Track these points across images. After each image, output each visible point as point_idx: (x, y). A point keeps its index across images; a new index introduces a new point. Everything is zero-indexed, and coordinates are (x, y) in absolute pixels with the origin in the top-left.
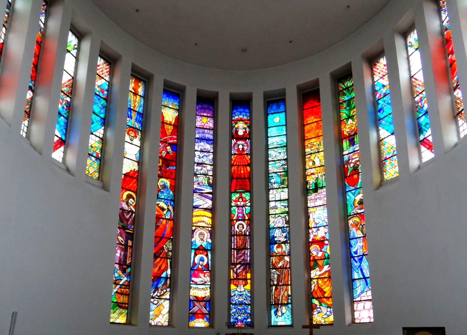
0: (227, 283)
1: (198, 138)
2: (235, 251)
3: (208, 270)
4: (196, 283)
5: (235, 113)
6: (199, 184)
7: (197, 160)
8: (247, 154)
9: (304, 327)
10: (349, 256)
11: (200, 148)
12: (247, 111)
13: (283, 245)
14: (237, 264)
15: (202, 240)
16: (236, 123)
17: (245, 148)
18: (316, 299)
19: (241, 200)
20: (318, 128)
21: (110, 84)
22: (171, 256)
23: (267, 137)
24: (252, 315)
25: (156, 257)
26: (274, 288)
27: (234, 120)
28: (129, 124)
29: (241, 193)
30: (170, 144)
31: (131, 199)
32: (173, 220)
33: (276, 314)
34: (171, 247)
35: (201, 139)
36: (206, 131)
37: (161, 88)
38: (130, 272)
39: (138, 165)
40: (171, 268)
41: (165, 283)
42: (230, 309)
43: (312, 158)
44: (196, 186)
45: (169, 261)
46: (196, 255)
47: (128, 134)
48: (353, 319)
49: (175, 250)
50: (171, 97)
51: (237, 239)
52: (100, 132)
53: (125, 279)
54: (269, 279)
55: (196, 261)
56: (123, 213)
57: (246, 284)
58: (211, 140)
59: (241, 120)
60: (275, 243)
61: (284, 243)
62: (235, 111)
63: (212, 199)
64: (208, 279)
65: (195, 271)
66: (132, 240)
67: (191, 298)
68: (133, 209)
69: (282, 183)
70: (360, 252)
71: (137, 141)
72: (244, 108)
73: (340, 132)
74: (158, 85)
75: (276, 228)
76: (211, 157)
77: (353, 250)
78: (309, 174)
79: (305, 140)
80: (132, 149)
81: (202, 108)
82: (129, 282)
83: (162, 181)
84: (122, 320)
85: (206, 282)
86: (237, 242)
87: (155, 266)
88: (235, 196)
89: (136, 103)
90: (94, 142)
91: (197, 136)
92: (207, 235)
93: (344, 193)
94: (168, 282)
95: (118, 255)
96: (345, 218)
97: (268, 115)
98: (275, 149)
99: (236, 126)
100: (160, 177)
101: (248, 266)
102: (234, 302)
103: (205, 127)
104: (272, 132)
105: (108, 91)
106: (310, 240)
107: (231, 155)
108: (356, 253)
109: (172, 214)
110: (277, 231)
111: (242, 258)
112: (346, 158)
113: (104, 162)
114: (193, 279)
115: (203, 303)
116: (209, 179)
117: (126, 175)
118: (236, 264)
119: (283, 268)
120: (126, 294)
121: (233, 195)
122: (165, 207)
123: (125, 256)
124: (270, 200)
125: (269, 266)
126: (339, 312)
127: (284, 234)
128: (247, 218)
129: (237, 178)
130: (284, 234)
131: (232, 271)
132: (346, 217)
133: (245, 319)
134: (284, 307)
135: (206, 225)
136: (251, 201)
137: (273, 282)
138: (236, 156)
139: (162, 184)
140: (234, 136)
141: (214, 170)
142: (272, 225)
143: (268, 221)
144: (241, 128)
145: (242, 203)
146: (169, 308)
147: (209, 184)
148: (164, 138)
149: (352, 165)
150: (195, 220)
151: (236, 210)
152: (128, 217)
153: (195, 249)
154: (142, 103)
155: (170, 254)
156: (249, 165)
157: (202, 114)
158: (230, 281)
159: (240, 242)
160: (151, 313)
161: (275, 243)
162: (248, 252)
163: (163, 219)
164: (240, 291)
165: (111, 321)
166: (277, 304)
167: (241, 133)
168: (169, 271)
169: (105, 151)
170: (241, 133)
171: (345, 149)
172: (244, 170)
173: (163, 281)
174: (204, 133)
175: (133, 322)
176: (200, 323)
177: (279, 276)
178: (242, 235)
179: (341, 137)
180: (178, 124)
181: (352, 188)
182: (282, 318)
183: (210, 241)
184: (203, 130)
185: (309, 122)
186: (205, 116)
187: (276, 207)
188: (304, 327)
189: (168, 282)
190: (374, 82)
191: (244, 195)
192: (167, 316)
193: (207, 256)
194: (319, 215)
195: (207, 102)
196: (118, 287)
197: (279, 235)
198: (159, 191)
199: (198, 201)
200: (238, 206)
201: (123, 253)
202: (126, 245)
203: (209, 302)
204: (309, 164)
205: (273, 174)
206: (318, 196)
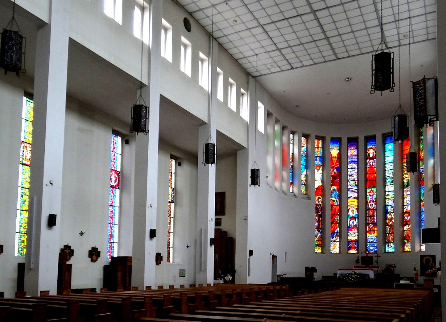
1: (349, 162)
2: (369, 218)
3: (356, 227)
4: (351, 234)
5: (368, 145)
6: (350, 186)
7: (349, 173)
8: (375, 167)
9: (380, 256)
11: (351, 166)
12: (374, 143)
13: (392, 214)
15: (353, 213)
16: (369, 150)
17: (374, 164)
19: (371, 192)
21: (307, 147)
22: (339, 222)
25: (332, 223)
26: (387, 234)
27: (368, 149)
28: (316, 164)
29: (371, 188)
30: (336, 168)
31: (320, 199)
32: (339, 205)
33: (388, 247)
34: (339, 218)
35: (351, 162)
36: (353, 157)
37: (330, 139)
38: (321, 231)
39: (322, 182)
40: (339, 228)
41: (337, 235)
44: (349, 187)
45: (338, 225)
46: (350, 220)
47: (316, 169)
49: (340, 220)
50: (335, 143)
51: (370, 212)
52: (304, 173)
53: (319, 234)
55: (351, 224)
56: (317, 206)
57: (374, 233)
58: (356, 161)
59: (371, 148)
60: (388, 213)
61: (393, 213)
64: (356, 231)
65: (349, 228)
67: (349, 240)
68: (321, 204)
71: (320, 171)
72: (373, 142)
74: (328, 140)
75: (389, 205)
76: (356, 170)
78: (405, 177)
80: (318, 175)
82: (321, 235)
83: (333, 188)
84: (320, 251)
85: (355, 233)
86: (370, 213)
87: (332, 227)
90: (303, 178)
91: (349, 161)
92: (355, 211)
94: (338, 234)
95: (316, 225)
96: (419, 201)
97: (385, 144)
98: (388, 164)
99: (369, 152)
100: (332, 185)
102: (369, 242)
103: (353, 155)
104: (387, 154)
105: (306, 151)
106: (405, 211)
108: (423, 219)
109: (338, 202)
110: (389, 207)
111: (372, 221)
113: (307, 186)
116: (356, 183)
118: (369, 224)
119: (392, 225)
120: (321, 241)
121: (368, 189)
122: (335, 200)
123: (319, 225)
124: (386, 191)
127: (393, 209)
128: (374, 201)
129: (370, 181)
130: (393, 209)
131: (368, 227)
133: (374, 249)
134: (392, 244)
135: (355, 206)
137: (387, 232)
138: (369, 168)
139: (333, 189)
141: (358, 178)
142: (387, 204)
145: (372, 193)
146: (339, 245)
147: (356, 185)
148: (333, 166)
150: (349, 204)
151: (369, 197)
152: (319, 207)
153: (350, 218)
154: (321, 151)
155: (338, 221)
157: (351, 148)
160: (331, 248)
161: (388, 213)
163: (334, 205)
164: (372, 237)
165: (315, 252)
166: (389, 242)
167: (371, 156)
168: (338, 229)
169: (307, 181)
170: (371, 156)
171: (421, 166)
172: (373, 176)
174: (352, 158)
175: (324, 252)
176: (353, 251)
177: (390, 229)
178: (372, 210)
183: (357, 213)
184: (352, 157)
185: (406, 149)
186: (353, 149)
187: (388, 195)
188: (380, 256)
189: (338, 234)
191: (373, 189)
192: (338, 249)
193: (356, 220)
195: (353, 142)
196: (317, 238)
197: (390, 209)
198: (332, 192)
199: (350, 194)
201: (318, 224)
203: (357, 242)
205: (388, 178)
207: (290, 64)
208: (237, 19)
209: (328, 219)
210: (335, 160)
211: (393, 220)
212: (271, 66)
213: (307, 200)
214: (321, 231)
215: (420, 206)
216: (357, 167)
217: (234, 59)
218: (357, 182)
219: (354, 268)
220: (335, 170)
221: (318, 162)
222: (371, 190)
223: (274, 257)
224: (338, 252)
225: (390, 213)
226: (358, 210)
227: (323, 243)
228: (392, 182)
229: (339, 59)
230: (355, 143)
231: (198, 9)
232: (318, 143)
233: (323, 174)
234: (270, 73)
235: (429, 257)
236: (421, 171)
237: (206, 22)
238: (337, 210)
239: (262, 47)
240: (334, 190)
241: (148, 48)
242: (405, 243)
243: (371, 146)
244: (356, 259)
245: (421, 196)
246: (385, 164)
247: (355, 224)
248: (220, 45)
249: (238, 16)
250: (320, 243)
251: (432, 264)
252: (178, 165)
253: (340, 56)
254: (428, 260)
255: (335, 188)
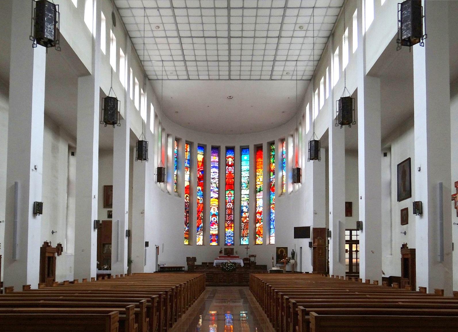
0: (224, 228)
4: (212, 229)
9: (249, 248)
10: (270, 220)
12: (233, 153)
13: (246, 213)
14: (228, 221)
16: (228, 159)
17: (232, 170)
18: (258, 235)
20: (262, 164)
23: (241, 166)
24: (233, 240)
30: (201, 171)
35: (214, 167)
36: (215, 163)
37: (197, 145)
42: (225, 238)
43: (259, 177)
44: (212, 188)
45: (202, 220)
46: (212, 217)
48: (270, 242)
53: (187, 228)
54: (241, 227)
55: (212, 220)
57: (232, 228)
59: (230, 157)
61: (247, 212)
62: (227, 153)
63: (218, 194)
64: (217, 227)
66: (188, 214)
68: (188, 201)
69: (247, 187)
70: (274, 218)
71: (188, 173)
72: (232, 151)
73: (270, 168)
74: (196, 146)
77: (271, 217)
79: (256, 169)
81: (213, 152)
88: (227, 192)
89: (187, 155)
91: (212, 166)
92: (216, 209)
93: (270, 194)
94: (202, 228)
97: (242, 155)
99: (228, 160)
101: (232, 221)
106: (257, 212)
107: (226, 174)
108: (272, 218)
110: (244, 207)
112: (271, 180)
114: (211, 227)
115: (215, 236)
117: (186, 187)
120: (188, 234)
121: (227, 191)
122: (200, 199)
123: (187, 220)
125: (241, 221)
126: (264, 241)
127: (247, 209)
128: (232, 202)
129: (228, 184)
130: (247, 209)
132: (270, 204)
136: (234, 194)
140: (227, 165)
141: (219, 181)
142: (242, 205)
143: (241, 203)
144: (230, 161)
147: (217, 187)
149: (273, 183)
150: (211, 203)
153: (212, 215)
155: (202, 217)
156: (234, 178)
157: (213, 155)
158: (226, 227)
159: (230, 212)
161: (243, 212)
162: (232, 216)
164: (229, 231)
166: (243, 236)
167: (230, 163)
168: (202, 224)
170: (230, 163)
173: (200, 228)
174: (214, 164)
175: (191, 244)
176: (214, 244)
177: (244, 225)
179: (270, 171)
180: (204, 161)
181: (273, 193)
182: (245, 242)
183: (217, 211)
187: (244, 197)
188: (249, 248)
189: (202, 228)
190: (283, 150)
191: (231, 192)
193: (216, 217)
194: (260, 202)
195: (216, 149)
197: (245, 209)
199: (212, 195)
200: (229, 197)
202: (187, 216)
203: (217, 236)
204: (258, 180)
205: (243, 183)
206: (260, 194)
207: (189, 75)
208: (161, 26)
209: (193, 216)
210: (200, 164)
211: (248, 219)
212: (171, 73)
213: (177, 197)
214: (188, 225)
215: (270, 209)
216: (218, 172)
217: (140, 59)
218: (218, 184)
219: (219, 258)
220: (200, 173)
221: (187, 165)
222: (230, 193)
223: (157, 248)
224: (202, 244)
225: (245, 213)
226: (218, 208)
227: (189, 236)
228: (247, 187)
229: (231, 80)
230: (217, 151)
231: (128, 6)
232: (187, 147)
233: (190, 175)
234: (167, 80)
235: (282, 249)
236: (271, 180)
237: (126, 20)
238: (201, 208)
239: (171, 55)
240: (199, 190)
241: (91, 36)
242: (256, 238)
243: (230, 155)
244: (220, 250)
245: (271, 201)
246: (241, 171)
247: (216, 221)
248: (133, 44)
249: (163, 23)
250: (187, 236)
251: (285, 255)
252: (71, 154)
253: (232, 77)
254: (282, 252)
255: (200, 188)
